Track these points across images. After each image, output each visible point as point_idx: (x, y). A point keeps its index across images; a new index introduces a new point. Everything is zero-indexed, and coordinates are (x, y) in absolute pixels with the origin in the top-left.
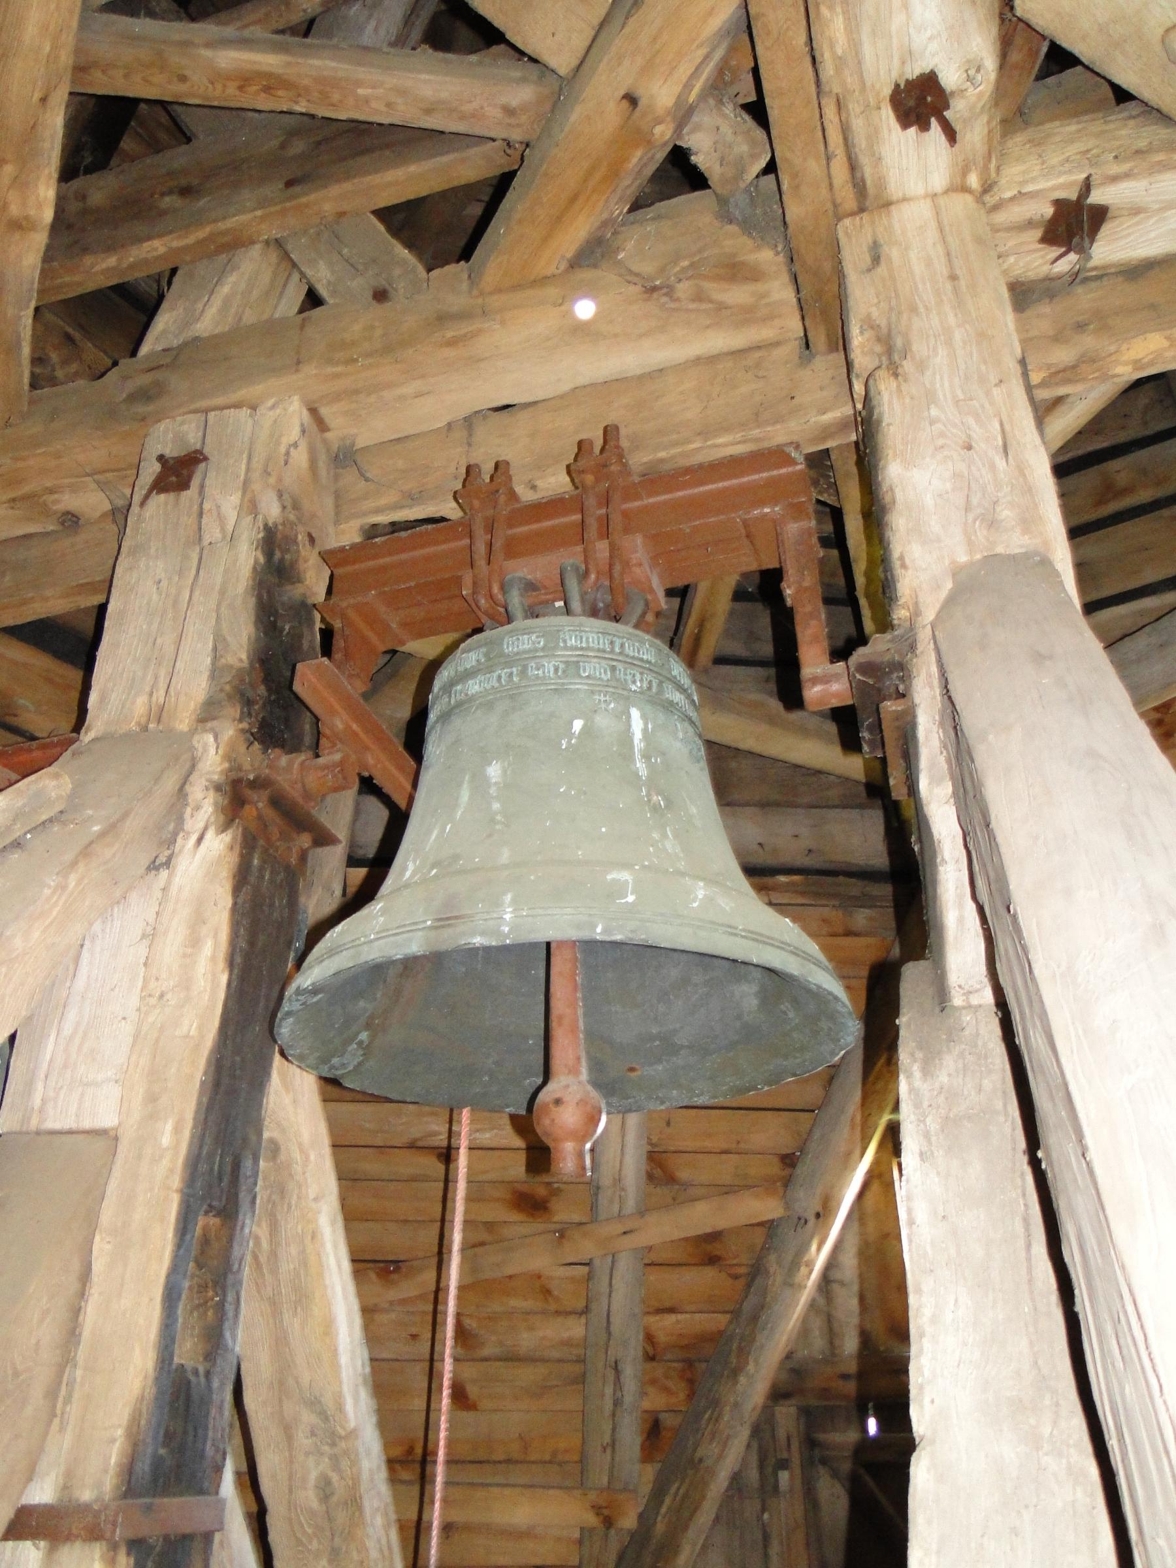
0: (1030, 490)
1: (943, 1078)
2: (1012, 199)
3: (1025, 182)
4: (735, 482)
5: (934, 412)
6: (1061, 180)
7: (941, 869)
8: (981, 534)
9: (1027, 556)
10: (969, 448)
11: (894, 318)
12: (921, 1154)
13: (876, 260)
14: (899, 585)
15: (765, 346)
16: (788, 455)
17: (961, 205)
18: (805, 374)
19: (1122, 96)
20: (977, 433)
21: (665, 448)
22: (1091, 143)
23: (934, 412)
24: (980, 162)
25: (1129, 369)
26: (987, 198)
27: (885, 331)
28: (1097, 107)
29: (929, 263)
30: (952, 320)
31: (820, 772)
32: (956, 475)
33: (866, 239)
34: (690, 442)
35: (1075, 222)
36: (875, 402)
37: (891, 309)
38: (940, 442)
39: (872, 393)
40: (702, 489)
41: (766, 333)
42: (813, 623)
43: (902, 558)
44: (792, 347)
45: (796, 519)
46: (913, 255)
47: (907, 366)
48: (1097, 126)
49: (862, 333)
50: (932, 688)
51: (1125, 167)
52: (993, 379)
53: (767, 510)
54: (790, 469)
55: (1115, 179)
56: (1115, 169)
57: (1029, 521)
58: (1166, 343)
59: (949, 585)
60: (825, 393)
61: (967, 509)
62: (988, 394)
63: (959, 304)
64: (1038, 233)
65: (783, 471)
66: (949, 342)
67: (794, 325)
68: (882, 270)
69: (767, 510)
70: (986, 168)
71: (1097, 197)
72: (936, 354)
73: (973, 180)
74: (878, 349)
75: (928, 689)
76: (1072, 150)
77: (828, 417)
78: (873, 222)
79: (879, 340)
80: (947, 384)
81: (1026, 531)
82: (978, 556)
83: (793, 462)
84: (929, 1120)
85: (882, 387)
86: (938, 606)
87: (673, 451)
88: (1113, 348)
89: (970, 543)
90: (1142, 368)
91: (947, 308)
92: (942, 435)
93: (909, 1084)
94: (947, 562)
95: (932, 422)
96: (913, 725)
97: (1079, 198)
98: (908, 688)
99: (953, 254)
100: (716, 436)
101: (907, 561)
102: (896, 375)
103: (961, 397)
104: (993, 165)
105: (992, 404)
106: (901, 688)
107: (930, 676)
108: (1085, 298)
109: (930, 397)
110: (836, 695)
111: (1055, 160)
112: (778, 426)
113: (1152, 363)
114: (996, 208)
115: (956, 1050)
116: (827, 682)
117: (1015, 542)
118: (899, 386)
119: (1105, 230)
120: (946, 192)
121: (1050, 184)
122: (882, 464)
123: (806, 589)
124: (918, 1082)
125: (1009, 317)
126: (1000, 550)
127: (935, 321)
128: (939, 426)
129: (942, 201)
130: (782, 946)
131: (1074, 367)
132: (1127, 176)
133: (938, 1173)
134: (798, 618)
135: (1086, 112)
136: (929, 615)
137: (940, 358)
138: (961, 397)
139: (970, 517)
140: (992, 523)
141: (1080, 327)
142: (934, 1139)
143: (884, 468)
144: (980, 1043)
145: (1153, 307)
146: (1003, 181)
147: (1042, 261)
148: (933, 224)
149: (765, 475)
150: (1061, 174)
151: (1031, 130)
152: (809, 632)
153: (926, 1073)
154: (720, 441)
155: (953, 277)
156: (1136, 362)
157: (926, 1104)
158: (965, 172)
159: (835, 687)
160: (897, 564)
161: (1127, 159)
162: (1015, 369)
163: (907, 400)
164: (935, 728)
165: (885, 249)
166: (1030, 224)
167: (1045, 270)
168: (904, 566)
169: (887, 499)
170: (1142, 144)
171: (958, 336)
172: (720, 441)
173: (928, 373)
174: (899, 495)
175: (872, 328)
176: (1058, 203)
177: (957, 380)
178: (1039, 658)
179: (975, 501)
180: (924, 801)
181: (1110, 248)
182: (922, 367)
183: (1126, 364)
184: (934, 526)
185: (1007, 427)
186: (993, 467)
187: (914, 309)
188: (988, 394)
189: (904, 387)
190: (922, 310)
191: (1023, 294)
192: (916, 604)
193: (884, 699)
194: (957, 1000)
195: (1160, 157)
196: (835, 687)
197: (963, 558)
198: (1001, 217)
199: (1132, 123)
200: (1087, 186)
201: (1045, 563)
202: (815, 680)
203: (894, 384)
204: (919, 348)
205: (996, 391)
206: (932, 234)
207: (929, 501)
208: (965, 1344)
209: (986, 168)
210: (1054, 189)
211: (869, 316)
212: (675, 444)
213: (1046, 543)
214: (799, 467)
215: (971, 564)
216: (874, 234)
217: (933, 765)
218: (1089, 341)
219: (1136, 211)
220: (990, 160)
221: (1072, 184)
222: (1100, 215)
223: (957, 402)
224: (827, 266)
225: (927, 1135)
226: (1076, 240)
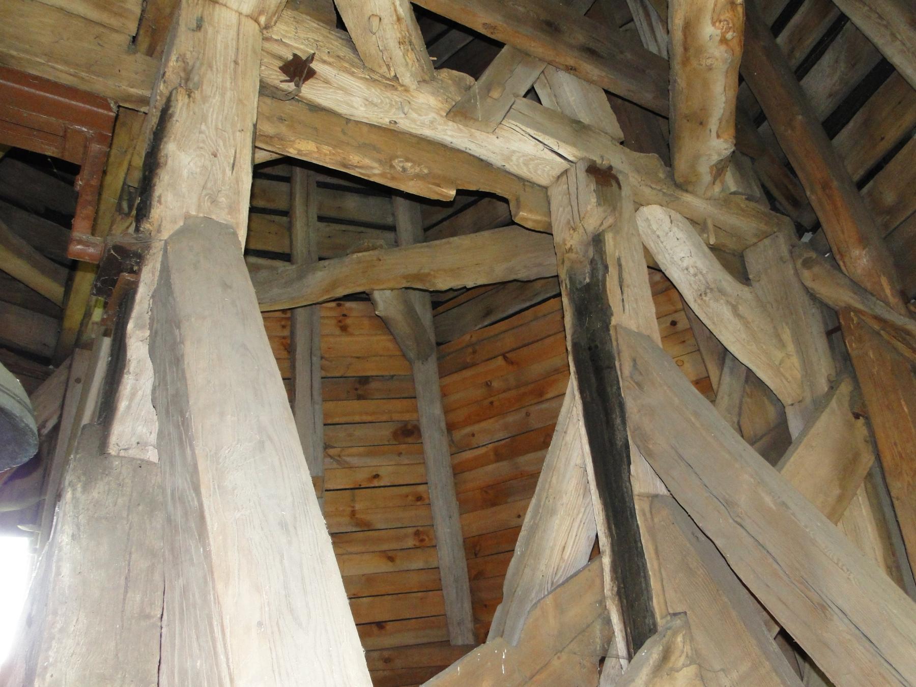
0: (238, 193)
1: (95, 494)
2: (276, 40)
3: (285, 36)
4: (67, 100)
5: (203, 127)
6: (302, 47)
7: (126, 376)
8: (207, 204)
9: (227, 227)
10: (215, 156)
11: (198, 64)
12: (73, 535)
13: (199, 27)
14: (152, 211)
15: (108, 28)
16: (109, 104)
17: (251, 28)
18: (130, 59)
19: (341, 25)
20: (222, 150)
21: (17, 50)
22: (321, 38)
23: (203, 127)
24: (270, 11)
25: (296, 152)
26: (265, 32)
27: (190, 68)
28: (327, 22)
29: (226, 47)
30: (228, 84)
31: (14, 279)
32: (204, 167)
33: (198, 12)
34: (37, 56)
35: (299, 69)
36: (172, 104)
37: (198, 58)
38: (201, 145)
39: (173, 98)
40: (42, 93)
41: (114, 22)
42: (90, 208)
43: (160, 197)
44: (123, 39)
45: (99, 142)
46: (220, 38)
47: (197, 94)
48: (325, 32)
49: (177, 61)
50: (153, 275)
51: (331, 60)
52: (239, 126)
53: (84, 129)
54: (106, 112)
55: (324, 62)
56: (326, 58)
57: (233, 209)
58: (316, 150)
59: (181, 224)
60: (137, 77)
61: (204, 188)
62: (234, 133)
63: (234, 78)
64: (281, 64)
65: (101, 111)
66: (223, 95)
67: (132, 28)
68: (200, 35)
69: (84, 129)
70: (271, 18)
71: (314, 65)
72: (214, 97)
73: (263, 20)
74: (182, 74)
75: (151, 275)
76: (311, 36)
77: (133, 91)
78: (204, 7)
79: (185, 70)
80: (215, 116)
81: (230, 213)
82: (201, 215)
83: (110, 109)
84: (80, 517)
85: (180, 98)
86: (171, 232)
87: (22, 55)
88: (293, 139)
89: (199, 207)
90: (301, 155)
91: (228, 76)
92: (203, 142)
93: (73, 494)
94: (184, 210)
95: (200, 132)
96: (135, 292)
97: (307, 60)
98: (140, 270)
99: (240, 50)
100: (57, 62)
101: (163, 200)
102: (189, 96)
103: (220, 127)
104: (274, 19)
105: (234, 139)
106: (135, 268)
107: (154, 268)
108: (289, 107)
109: (204, 119)
110: (90, 255)
111: (302, 35)
112: (101, 79)
113: (305, 155)
114: (266, 39)
115: (106, 480)
116: (88, 246)
117: (221, 216)
118: (189, 103)
119: (310, 82)
120: (247, 16)
121: (296, 45)
122: (165, 139)
123: (92, 186)
124: (79, 493)
125: (254, 99)
126: (214, 217)
127: (220, 80)
128: (204, 136)
129: (243, 19)
130: (14, 396)
131: (271, 137)
132: (329, 64)
133: (81, 548)
134: (80, 200)
135: (323, 22)
136: (165, 235)
137: (216, 100)
138: (220, 127)
139: (204, 193)
140: (214, 201)
141: (281, 119)
142: (82, 528)
143: (166, 143)
144: (121, 478)
145: (316, 129)
146: (275, 29)
147: (276, 78)
148: (235, 29)
149: (88, 107)
150: (302, 43)
151: (295, 12)
152: (85, 212)
153: (85, 489)
154: (59, 67)
155: (236, 63)
156: (299, 151)
157: (81, 507)
158: (261, 13)
159: (91, 250)
160: (155, 199)
161: (332, 57)
162: (251, 128)
163: (191, 113)
164: (148, 298)
165: (206, 25)
166: (280, 58)
167: (277, 82)
168: (159, 202)
169: (162, 160)
170: (341, 54)
171: (229, 94)
172: (59, 67)
173: (207, 105)
174: (170, 162)
175: (184, 62)
176: (295, 55)
177: (221, 117)
178: (226, 286)
179: (209, 185)
180: (128, 336)
181: (309, 91)
182: (205, 99)
183: (295, 149)
184: (184, 188)
185: (238, 156)
186: (224, 172)
187: (210, 66)
188: (234, 133)
189: (192, 104)
190: (215, 69)
191: (265, 90)
192: (160, 226)
193: (122, 271)
194: (112, 450)
195: (346, 65)
196: (91, 250)
197: (194, 213)
198: (267, 45)
199: (340, 41)
200: (312, 58)
201: (235, 234)
202: (80, 242)
203: (186, 100)
204: (207, 89)
205: (238, 134)
206: (233, 33)
207: (185, 173)
208: (78, 644)
209: (271, 18)
210: (297, 49)
211: (185, 55)
212: (26, 51)
213: (237, 224)
214: (112, 114)
215: (197, 217)
216: (203, 12)
217: (139, 317)
218: (283, 129)
219: (327, 82)
220: (275, 15)
221: (304, 52)
222: (311, 74)
223: (217, 129)
224: (168, 10)
225: (78, 526)
226: (297, 78)
